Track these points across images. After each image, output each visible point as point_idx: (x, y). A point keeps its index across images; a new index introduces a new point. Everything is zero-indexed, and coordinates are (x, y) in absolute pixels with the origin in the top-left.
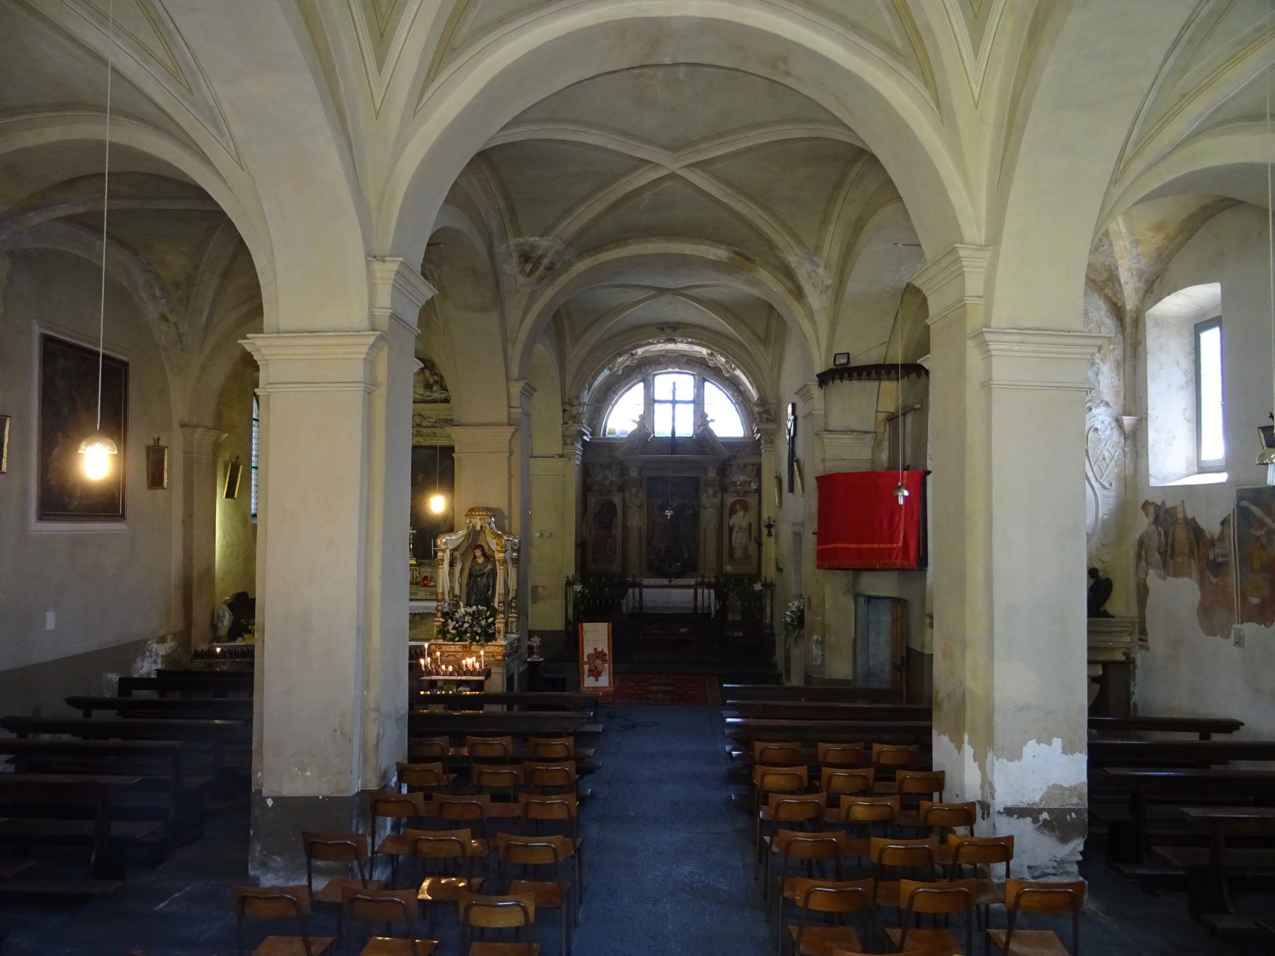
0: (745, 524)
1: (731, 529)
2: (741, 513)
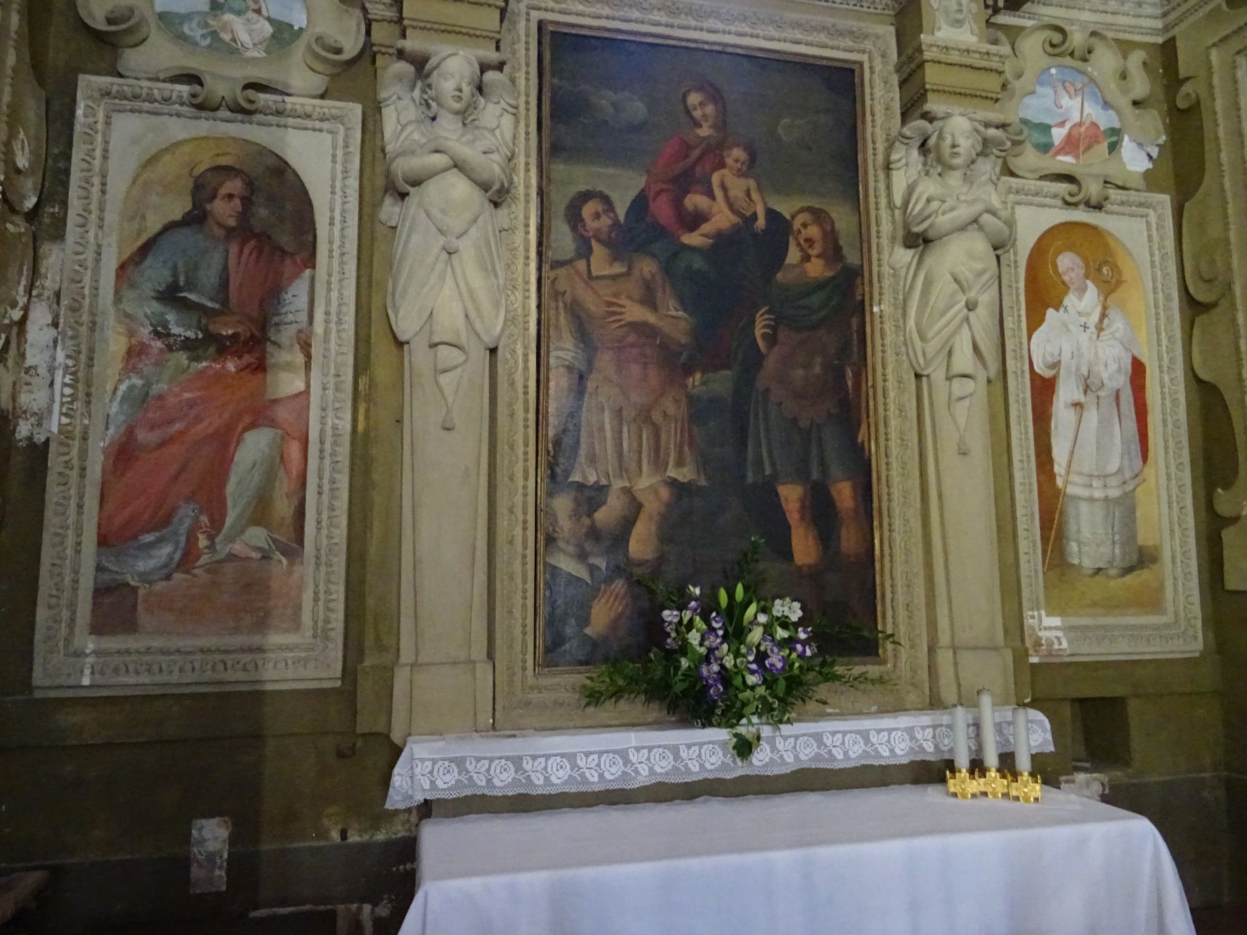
0: (1110, 363)
1: (1043, 389)
2: (1083, 302)
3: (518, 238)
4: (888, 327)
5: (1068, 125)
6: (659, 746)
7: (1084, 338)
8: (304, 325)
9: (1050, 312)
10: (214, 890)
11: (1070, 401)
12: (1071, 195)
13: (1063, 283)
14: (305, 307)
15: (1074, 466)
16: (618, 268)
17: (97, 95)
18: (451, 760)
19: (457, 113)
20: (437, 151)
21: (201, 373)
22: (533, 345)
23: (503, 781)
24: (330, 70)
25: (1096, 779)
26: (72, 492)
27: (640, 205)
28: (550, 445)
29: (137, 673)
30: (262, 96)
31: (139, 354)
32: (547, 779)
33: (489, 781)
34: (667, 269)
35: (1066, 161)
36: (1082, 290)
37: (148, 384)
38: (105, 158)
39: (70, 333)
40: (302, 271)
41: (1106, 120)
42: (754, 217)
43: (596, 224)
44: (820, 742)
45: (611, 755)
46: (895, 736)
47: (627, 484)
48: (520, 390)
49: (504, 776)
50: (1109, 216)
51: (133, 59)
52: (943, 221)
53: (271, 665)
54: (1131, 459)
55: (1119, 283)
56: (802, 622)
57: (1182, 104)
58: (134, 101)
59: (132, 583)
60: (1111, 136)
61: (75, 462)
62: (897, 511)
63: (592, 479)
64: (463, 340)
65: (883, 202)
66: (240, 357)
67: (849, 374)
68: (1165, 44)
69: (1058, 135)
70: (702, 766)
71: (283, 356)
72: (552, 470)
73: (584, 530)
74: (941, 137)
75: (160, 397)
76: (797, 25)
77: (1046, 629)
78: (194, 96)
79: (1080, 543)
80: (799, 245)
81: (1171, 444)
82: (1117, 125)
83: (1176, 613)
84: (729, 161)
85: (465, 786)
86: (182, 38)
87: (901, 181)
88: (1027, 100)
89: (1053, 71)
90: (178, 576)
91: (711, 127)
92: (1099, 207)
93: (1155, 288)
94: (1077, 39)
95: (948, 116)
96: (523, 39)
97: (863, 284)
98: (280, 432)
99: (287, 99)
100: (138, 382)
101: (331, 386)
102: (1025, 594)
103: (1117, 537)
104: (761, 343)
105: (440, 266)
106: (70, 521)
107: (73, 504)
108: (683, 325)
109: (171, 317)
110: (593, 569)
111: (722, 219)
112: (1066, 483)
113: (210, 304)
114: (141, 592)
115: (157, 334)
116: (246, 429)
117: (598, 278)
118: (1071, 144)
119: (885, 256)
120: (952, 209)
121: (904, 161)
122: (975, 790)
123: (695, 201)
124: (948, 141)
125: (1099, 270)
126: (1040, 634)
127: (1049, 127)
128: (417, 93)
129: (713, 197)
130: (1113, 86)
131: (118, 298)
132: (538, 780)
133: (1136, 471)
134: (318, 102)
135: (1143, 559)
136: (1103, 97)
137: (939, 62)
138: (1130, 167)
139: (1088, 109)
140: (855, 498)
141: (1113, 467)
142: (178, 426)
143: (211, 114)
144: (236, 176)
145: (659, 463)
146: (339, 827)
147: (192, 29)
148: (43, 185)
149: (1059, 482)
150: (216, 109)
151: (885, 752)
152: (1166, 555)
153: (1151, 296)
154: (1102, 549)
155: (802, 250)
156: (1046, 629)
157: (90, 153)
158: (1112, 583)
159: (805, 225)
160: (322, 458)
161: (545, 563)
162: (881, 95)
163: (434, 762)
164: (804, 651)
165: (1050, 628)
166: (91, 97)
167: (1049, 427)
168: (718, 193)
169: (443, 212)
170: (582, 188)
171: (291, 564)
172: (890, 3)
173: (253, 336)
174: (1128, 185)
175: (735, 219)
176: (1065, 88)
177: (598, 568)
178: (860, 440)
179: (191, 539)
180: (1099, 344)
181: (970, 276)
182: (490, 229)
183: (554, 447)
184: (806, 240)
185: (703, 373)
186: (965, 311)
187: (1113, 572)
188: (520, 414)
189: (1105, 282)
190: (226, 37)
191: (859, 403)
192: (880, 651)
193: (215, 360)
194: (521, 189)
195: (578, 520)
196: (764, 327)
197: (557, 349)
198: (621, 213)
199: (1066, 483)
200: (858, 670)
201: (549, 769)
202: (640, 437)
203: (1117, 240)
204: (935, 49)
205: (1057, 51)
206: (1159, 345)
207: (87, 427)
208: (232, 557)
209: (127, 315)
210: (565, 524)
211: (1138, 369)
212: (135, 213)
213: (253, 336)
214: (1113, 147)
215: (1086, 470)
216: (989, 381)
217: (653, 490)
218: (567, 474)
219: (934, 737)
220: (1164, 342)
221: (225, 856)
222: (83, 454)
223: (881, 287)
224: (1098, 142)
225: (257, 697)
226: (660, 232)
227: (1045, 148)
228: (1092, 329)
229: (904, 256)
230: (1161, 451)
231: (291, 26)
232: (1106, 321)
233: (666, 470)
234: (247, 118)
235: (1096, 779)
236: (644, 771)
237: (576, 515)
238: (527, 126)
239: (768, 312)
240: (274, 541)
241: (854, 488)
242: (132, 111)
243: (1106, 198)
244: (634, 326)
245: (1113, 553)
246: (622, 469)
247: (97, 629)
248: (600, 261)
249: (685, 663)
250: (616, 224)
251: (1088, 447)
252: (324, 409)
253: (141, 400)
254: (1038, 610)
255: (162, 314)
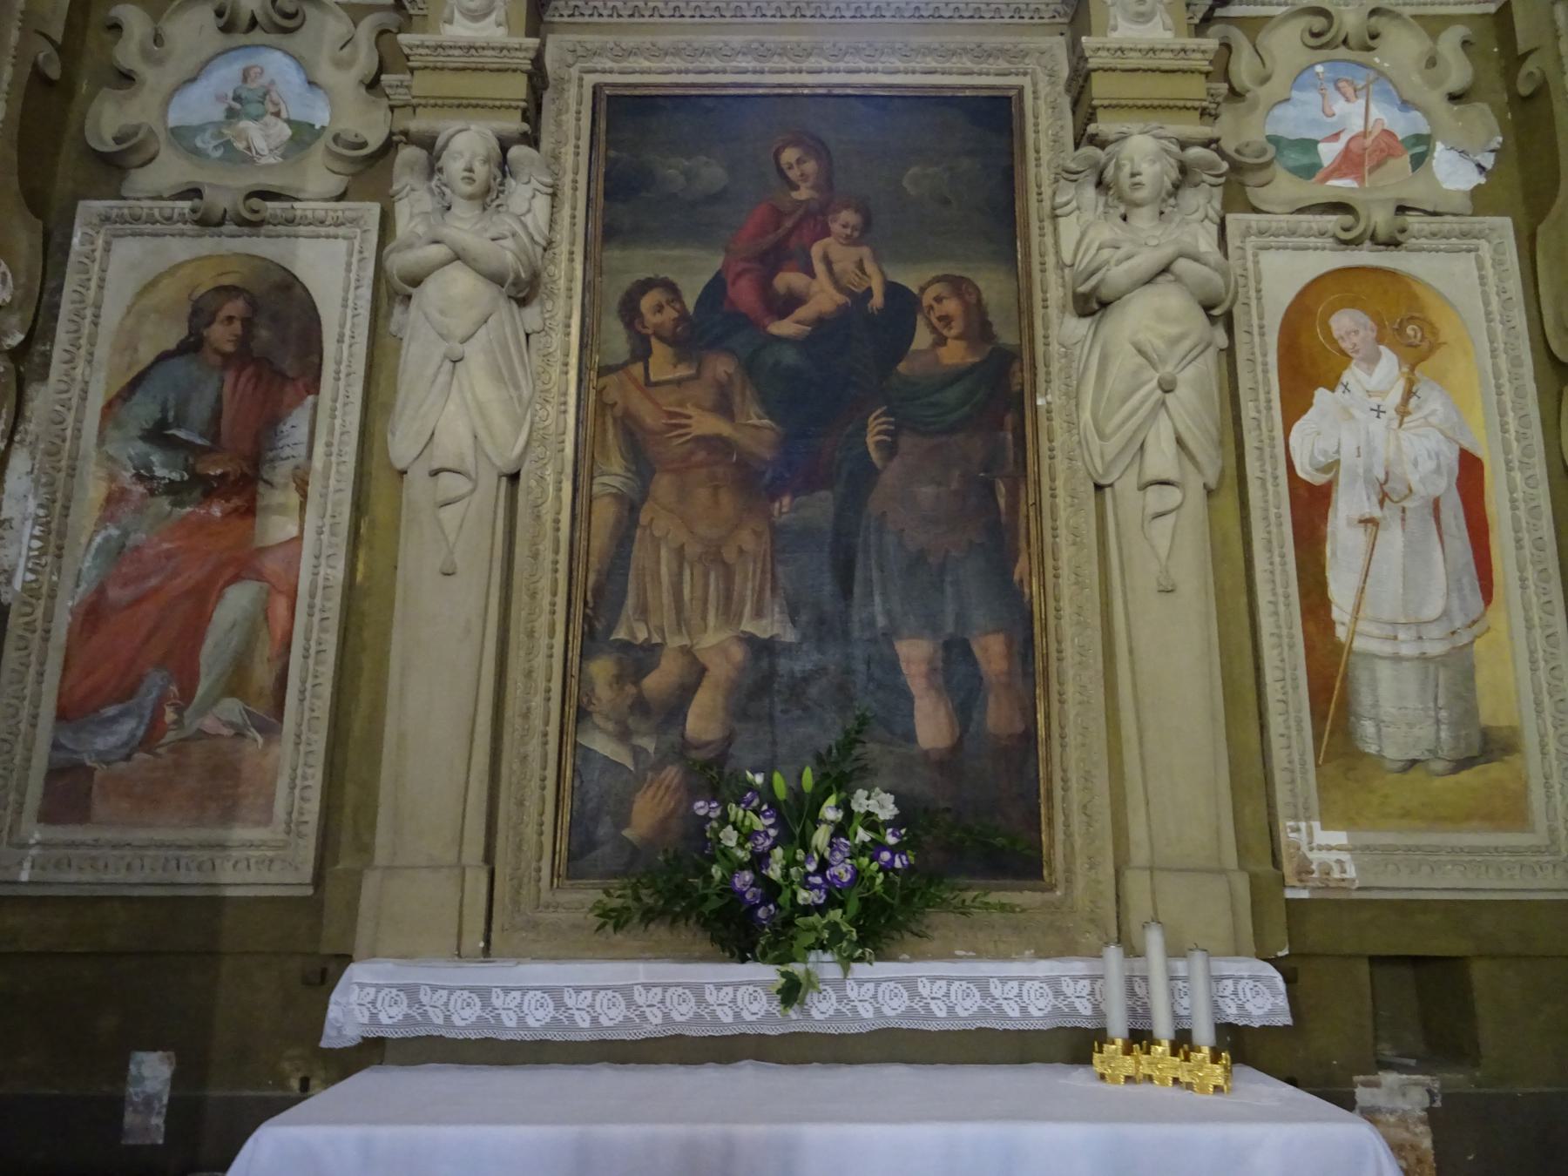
0: (1423, 456)
1: (1311, 504)
2: (1376, 377)
3: (556, 339)
4: (1058, 423)
5: (1344, 139)
6: (678, 985)
7: (1377, 426)
8: (301, 460)
9: (1321, 395)
10: (148, 1142)
11: (1357, 517)
12: (1346, 230)
13: (1343, 352)
14: (305, 439)
15: (1366, 610)
16: (683, 371)
17: (96, 220)
18: (400, 988)
19: (471, 197)
20: (436, 242)
21: (184, 519)
22: (569, 470)
23: (464, 1019)
24: (350, 169)
25: (1416, 1084)
26: (33, 658)
27: (716, 290)
28: (589, 594)
29: (81, 869)
30: (270, 204)
31: (119, 501)
32: (521, 1020)
33: (447, 1018)
34: (750, 367)
35: (1343, 186)
36: (1372, 360)
37: (125, 534)
38: (101, 288)
39: (44, 480)
40: (303, 398)
41: (1404, 125)
42: (869, 292)
43: (658, 319)
44: (914, 993)
45: (610, 993)
46: (1029, 988)
47: (686, 641)
48: (549, 525)
49: (467, 1013)
50: (1413, 256)
51: (144, 180)
52: (1117, 275)
53: (231, 864)
54: (1463, 599)
55: (1433, 348)
56: (894, 823)
57: (1524, 89)
58: (133, 224)
59: (89, 763)
60: (1415, 145)
61: (39, 624)
62: (1071, 673)
63: (642, 636)
64: (469, 465)
65: (1051, 260)
66: (227, 501)
67: (1001, 488)
68: (1500, 10)
69: (1328, 153)
70: (737, 1015)
71: (275, 497)
72: (591, 627)
73: (629, 702)
74: (1118, 167)
75: (137, 548)
76: (928, 51)
77: (1320, 848)
78: (194, 211)
79: (1378, 723)
80: (930, 324)
81: (1530, 574)
82: (1425, 129)
83: (1552, 830)
84: (835, 227)
85: (418, 1024)
86: (196, 152)
87: (1075, 232)
88: (1278, 111)
89: (1319, 69)
90: (140, 756)
91: (813, 188)
92: (1393, 243)
93: (1493, 351)
94: (1351, 20)
95: (1124, 137)
96: (573, 108)
97: (1022, 370)
98: (266, 585)
99: (297, 205)
100: (114, 532)
101: (326, 529)
102: (1282, 794)
103: (1443, 714)
104: (874, 455)
105: (443, 378)
106: (27, 692)
107: (32, 671)
108: (768, 436)
109: (156, 458)
110: (637, 752)
111: (823, 298)
112: (1353, 633)
113: (199, 441)
114: (98, 775)
115: (139, 477)
116: (229, 583)
117: (657, 384)
118: (1350, 162)
119: (1054, 332)
120: (1129, 258)
121: (1074, 204)
122: (1131, 1072)
123: (788, 280)
124: (1127, 170)
125: (1400, 330)
126: (1311, 855)
127: (1314, 143)
128: (433, 183)
129: (812, 274)
130: (1416, 78)
131: (102, 439)
132: (510, 1021)
133: (1474, 617)
134: (333, 205)
135: (1491, 746)
136: (1401, 97)
137: (1114, 70)
138: (1448, 185)
139: (1375, 113)
140: (1009, 656)
141: (1433, 608)
142: (153, 582)
143: (215, 230)
144: (237, 297)
145: (729, 611)
146: (300, 1075)
147: (205, 142)
148: (35, 320)
149: (1341, 633)
150: (220, 223)
151: (1014, 1012)
152: (1530, 741)
153: (1488, 362)
154: (1417, 731)
155: (934, 329)
156: (1320, 848)
157: (85, 284)
158: (1438, 783)
159: (938, 299)
160: (311, 615)
161: (576, 745)
162: (1046, 126)
163: (379, 988)
164: (892, 860)
165: (1329, 848)
166: (89, 224)
167: (1322, 553)
168: (819, 267)
169: (442, 312)
170: (642, 276)
171: (268, 742)
172: (1060, 8)
173: (244, 475)
174: (1439, 209)
175: (841, 299)
176: (1338, 89)
177: (646, 750)
178: (1016, 577)
179: (158, 712)
180: (1402, 434)
181: (1160, 345)
182: (508, 330)
183: (594, 596)
184: (940, 319)
185: (794, 497)
186: (1159, 393)
187: (1438, 766)
188: (547, 556)
189: (1410, 345)
190: (240, 146)
191: (1016, 528)
192: (1045, 872)
193: (199, 504)
194: (562, 283)
195: (622, 689)
196: (879, 433)
197: (602, 474)
198: (690, 302)
199: (1353, 633)
200: (994, 898)
201: (525, 1008)
202: (706, 586)
203: (1428, 286)
204: (1105, 54)
205: (1324, 39)
206: (1505, 431)
207: (56, 584)
208: (202, 734)
209: (110, 458)
210: (603, 693)
211: (1470, 469)
212: (127, 342)
213: (244, 475)
214: (1419, 161)
215: (1386, 616)
216: (1210, 493)
217: (721, 649)
218: (610, 629)
219: (1092, 993)
220: (1512, 426)
221: (165, 1100)
222: (49, 616)
223: (1048, 373)
224: (1391, 155)
225: (215, 904)
226: (740, 321)
227: (1309, 171)
228: (1392, 413)
229: (1078, 327)
230: (1514, 584)
231: (312, 126)
232: (1413, 401)
233: (739, 623)
234: (254, 230)
235: (1416, 1084)
236: (655, 1017)
237: (619, 679)
238: (574, 208)
239: (884, 414)
240: (247, 712)
241: (1009, 644)
242: (134, 235)
243: (1403, 231)
244: (704, 441)
245: (1438, 739)
246: (681, 622)
247: (47, 816)
248: (663, 365)
249: (716, 871)
250: (683, 317)
251: (1388, 587)
252: (317, 557)
253: (117, 552)
254: (1308, 819)
255: (148, 455)
